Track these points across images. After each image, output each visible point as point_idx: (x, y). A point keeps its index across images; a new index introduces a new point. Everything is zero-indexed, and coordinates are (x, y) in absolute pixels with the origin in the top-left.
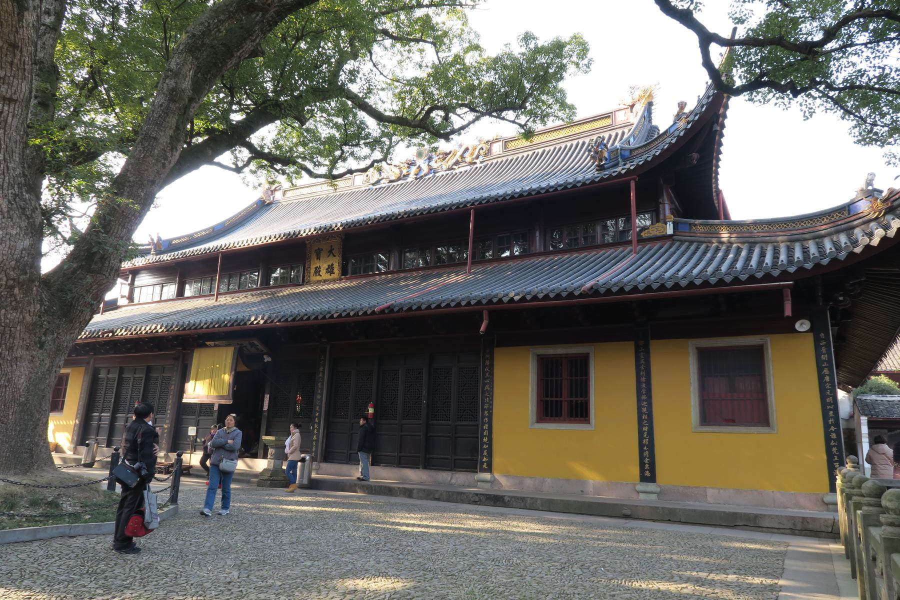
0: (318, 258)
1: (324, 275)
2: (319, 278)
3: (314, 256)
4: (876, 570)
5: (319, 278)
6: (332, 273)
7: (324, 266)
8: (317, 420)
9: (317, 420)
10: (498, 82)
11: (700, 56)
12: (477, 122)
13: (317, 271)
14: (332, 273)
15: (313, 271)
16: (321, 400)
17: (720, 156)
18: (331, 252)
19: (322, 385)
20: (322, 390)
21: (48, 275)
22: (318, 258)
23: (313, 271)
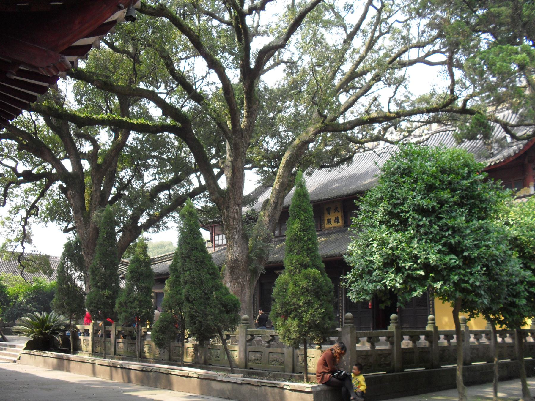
0: (329, 213)
1: (333, 224)
2: (330, 226)
3: (326, 213)
4: (227, 54)
5: (330, 226)
6: (338, 222)
7: (333, 219)
8: (341, 311)
9: (341, 311)
10: (320, 25)
11: (269, 71)
12: (276, 68)
13: (329, 221)
14: (338, 222)
15: (326, 222)
16: (342, 300)
17: (31, 238)
18: (336, 210)
19: (342, 292)
20: (342, 295)
21: (246, 196)
22: (329, 213)
23: (326, 222)
